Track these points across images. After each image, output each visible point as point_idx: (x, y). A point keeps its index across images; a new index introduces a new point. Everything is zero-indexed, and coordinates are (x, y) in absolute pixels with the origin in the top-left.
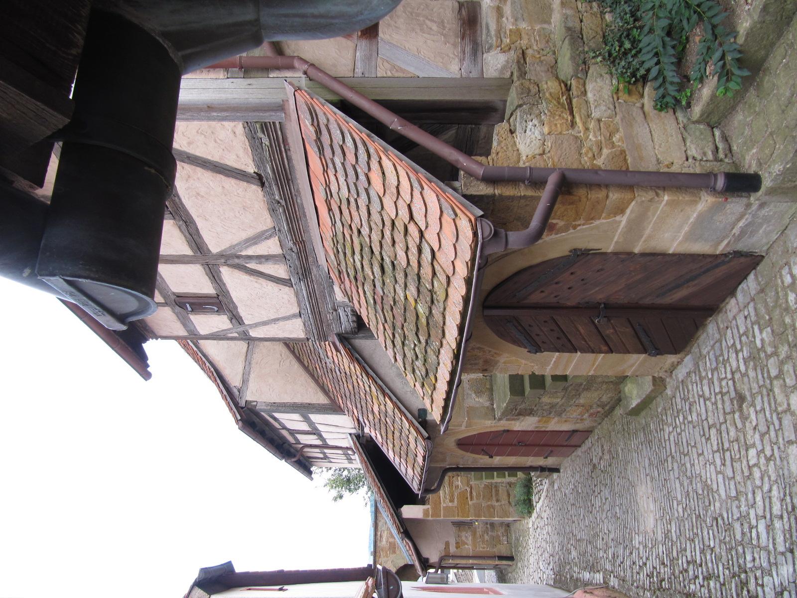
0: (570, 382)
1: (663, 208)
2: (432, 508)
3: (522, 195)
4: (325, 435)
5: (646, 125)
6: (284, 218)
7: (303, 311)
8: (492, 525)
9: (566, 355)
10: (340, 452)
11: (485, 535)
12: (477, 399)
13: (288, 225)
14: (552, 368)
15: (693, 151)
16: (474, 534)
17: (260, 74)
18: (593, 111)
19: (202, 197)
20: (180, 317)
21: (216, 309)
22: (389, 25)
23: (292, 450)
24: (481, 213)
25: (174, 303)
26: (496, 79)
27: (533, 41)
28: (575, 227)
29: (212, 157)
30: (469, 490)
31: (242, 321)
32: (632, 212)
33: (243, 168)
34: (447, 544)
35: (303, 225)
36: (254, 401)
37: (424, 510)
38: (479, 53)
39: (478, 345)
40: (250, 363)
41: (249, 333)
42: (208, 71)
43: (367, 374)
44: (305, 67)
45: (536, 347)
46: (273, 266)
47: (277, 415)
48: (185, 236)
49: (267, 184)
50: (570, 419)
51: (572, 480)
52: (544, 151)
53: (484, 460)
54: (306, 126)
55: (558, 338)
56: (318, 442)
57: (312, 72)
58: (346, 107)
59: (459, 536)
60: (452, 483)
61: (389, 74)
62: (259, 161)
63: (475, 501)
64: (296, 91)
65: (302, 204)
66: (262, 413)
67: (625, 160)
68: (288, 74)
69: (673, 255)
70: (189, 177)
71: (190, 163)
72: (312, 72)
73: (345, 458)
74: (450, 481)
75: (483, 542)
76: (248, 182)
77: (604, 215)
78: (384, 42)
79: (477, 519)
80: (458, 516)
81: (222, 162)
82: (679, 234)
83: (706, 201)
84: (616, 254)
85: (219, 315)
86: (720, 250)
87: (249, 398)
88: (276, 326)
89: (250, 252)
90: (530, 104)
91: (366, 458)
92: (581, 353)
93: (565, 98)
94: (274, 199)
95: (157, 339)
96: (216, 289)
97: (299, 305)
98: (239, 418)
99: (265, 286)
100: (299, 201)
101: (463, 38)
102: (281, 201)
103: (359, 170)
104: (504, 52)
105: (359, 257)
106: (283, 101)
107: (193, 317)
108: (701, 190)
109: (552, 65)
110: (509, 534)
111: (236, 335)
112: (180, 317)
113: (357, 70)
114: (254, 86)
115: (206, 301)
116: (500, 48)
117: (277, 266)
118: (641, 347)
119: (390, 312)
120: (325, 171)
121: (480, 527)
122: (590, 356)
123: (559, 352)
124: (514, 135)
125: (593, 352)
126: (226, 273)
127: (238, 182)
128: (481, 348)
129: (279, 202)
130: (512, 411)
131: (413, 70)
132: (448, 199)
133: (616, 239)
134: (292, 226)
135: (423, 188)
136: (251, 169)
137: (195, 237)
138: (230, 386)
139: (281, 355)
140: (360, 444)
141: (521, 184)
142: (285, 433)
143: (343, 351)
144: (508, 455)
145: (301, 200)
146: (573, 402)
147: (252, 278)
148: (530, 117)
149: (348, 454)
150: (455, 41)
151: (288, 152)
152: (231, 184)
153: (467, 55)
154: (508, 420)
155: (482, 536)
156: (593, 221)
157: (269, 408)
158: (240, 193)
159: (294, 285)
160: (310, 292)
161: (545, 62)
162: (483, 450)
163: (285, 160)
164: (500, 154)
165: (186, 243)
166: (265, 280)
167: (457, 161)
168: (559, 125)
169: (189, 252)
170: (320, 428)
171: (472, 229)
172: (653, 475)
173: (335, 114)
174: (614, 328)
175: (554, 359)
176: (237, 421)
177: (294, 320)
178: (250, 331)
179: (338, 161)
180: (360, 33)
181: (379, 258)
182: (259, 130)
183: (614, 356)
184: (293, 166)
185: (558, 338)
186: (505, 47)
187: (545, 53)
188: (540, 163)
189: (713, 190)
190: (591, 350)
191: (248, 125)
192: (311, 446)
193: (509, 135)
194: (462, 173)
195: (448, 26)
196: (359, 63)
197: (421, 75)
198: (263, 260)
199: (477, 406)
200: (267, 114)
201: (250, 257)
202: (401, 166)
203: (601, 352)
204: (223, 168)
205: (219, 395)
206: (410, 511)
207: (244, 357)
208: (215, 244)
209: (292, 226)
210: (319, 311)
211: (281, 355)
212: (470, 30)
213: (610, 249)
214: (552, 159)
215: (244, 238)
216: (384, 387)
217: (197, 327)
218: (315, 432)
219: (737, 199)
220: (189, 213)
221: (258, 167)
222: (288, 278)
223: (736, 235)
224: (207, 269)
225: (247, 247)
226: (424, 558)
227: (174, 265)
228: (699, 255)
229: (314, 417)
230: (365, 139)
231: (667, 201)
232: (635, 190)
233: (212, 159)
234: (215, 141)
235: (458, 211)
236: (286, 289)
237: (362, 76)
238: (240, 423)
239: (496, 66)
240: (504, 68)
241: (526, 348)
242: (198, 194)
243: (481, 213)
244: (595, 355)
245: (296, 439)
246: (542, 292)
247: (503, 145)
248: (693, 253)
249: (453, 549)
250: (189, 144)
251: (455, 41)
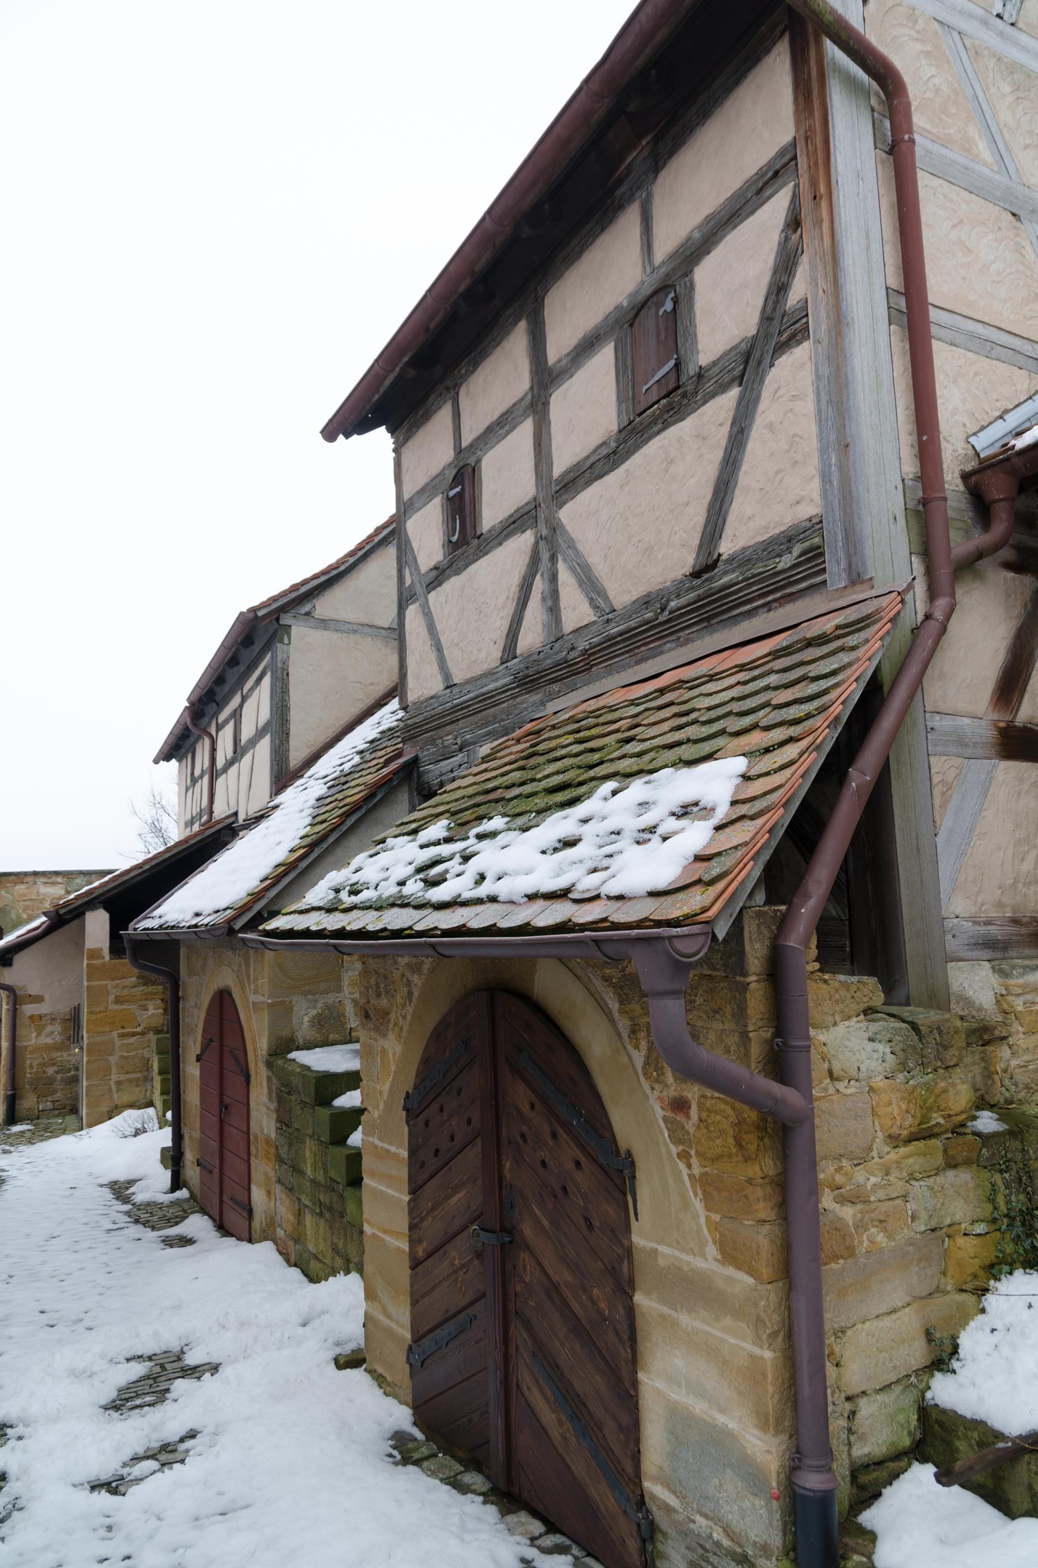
0: (349, 1192)
1: (744, 1349)
2: (104, 964)
3: (751, 1035)
4: (233, 770)
5: (907, 1299)
6: (632, 624)
7: (456, 690)
8: (75, 1080)
9: (404, 1173)
10: (205, 803)
11: (56, 1068)
12: (306, 1019)
13: (621, 635)
14: (376, 1147)
15: (866, 1408)
16: (58, 1047)
17: (915, 538)
18: (922, 1183)
19: (666, 470)
20: (437, 481)
21: (455, 539)
22: (1021, 780)
23: (205, 720)
24: (721, 936)
25: (461, 464)
26: (947, 986)
27: (1025, 1058)
28: (684, 1156)
29: (746, 473)
30: (139, 1029)
31: (434, 588)
32: (729, 1280)
33: (728, 531)
34: (38, 999)
35: (622, 663)
36: (289, 640)
37: (101, 949)
38: (987, 954)
39: (416, 993)
40: (355, 631)
41: (412, 603)
42: (912, 445)
43: (347, 815)
44: (939, 615)
45: (416, 1107)
46: (540, 622)
47: (267, 680)
48: (588, 457)
49: (698, 581)
50: (273, 1201)
51: (155, 1218)
52: (838, 1079)
53: (192, 1046)
54: (834, 619)
55: (437, 1151)
56: (220, 762)
57: (933, 626)
58: (873, 698)
59: (53, 1019)
60: (151, 999)
61: (936, 779)
62: (743, 559)
63: (118, 1043)
64: (899, 593)
65: (662, 653)
66: (269, 655)
67: (837, 1257)
68: (920, 588)
69: (635, 1383)
70: (704, 438)
71: (730, 436)
72: (933, 626)
73: (194, 814)
74: (155, 994)
75: (42, 1065)
76: (700, 546)
77: (716, 1217)
78: (992, 770)
79: (85, 1047)
80: (89, 1013)
81: (737, 492)
82: (684, 1391)
83: (765, 1449)
84: (629, 1251)
85: (443, 546)
86: (654, 1489)
87: (295, 631)
88: (427, 648)
89: (565, 576)
90: (922, 1049)
91: (193, 842)
92: (409, 1202)
93: (941, 1121)
94: (668, 600)
95: (394, 451)
96: (490, 531)
97: (468, 682)
98: (260, 614)
99: (501, 615)
100: (668, 646)
101: (1015, 921)
102: (666, 613)
103: (762, 713)
104: (998, 1001)
105: (574, 751)
106: (871, 579)
107: (437, 501)
108: (791, 1437)
109: (987, 1097)
110: (57, 1112)
111: (408, 581)
112: (437, 481)
113: (937, 718)
114: (892, 526)
115: (468, 519)
116: (1004, 992)
117: (539, 628)
118: (427, 1328)
119: (474, 816)
120: (742, 668)
121: (70, 1058)
122: (402, 1222)
123: (410, 1157)
124: (862, 1017)
125: (412, 1227)
126: (523, 542)
127: (700, 528)
128: (410, 1001)
129: (663, 610)
130: (286, 1086)
131: (946, 822)
132: (741, 865)
133: (662, 1249)
134: (618, 643)
135: (752, 818)
136: (727, 547)
137: (587, 475)
138: (314, 598)
139: (371, 684)
140: (219, 831)
141: (772, 1030)
142: (236, 700)
143: (385, 771)
144: (201, 1088)
145: (670, 650)
146: (308, 1203)
147: (514, 588)
148: (897, 1049)
149: (201, 818)
150: (1006, 906)
151: (765, 609)
152: (697, 516)
153: (983, 929)
154: (269, 1079)
155: (52, 1062)
156: (700, 1195)
157: (279, 665)
158: (677, 536)
159: (505, 665)
160: (493, 696)
161: (990, 1082)
162: (211, 1040)
163: (749, 607)
164: (825, 987)
165: (575, 460)
166: (512, 612)
167: (807, 896)
168: (889, 1109)
169: (558, 470)
170: (247, 759)
171: (687, 917)
172: (163, 1378)
173: (869, 659)
174: (463, 1266)
175: (393, 1149)
176: (253, 610)
177: (439, 677)
178: (417, 604)
179: (773, 679)
180: (1002, 725)
181: (581, 779)
182: (807, 544)
183: (403, 1272)
184: (736, 624)
185: (437, 1151)
186: (1009, 1004)
187: (1007, 1082)
188: (818, 1070)
189: (795, 1464)
190: (415, 1222)
191: (816, 525)
192: (213, 750)
193: (862, 1007)
194: (783, 908)
195: (1031, 892)
196: (950, 723)
197: (940, 840)
198: (550, 603)
199: (294, 1020)
200: (841, 554)
201: (553, 578)
202: (793, 775)
203: (413, 1242)
204: (725, 496)
205: (298, 580)
206: (97, 925)
207: (366, 621)
208: (572, 514)
209: (618, 643)
210: (458, 720)
211: (371, 684)
212: (1029, 935)
213: (638, 1240)
214: (823, 1097)
215: (590, 560)
216: (325, 845)
217: (419, 514)
218: (239, 751)
219: (777, 1523)
220: (633, 454)
221: (731, 559)
222: (518, 652)
223: (692, 1525)
224: (527, 509)
225: (573, 570)
226: (11, 959)
227: (532, 450)
228: (637, 1441)
229: (265, 745)
230: (832, 709)
231: (762, 1358)
232: (780, 1284)
233: (741, 473)
234: (777, 473)
235: (720, 886)
236: (497, 653)
237: (929, 727)
238: (252, 615)
239: (970, 986)
240: (969, 1002)
241: (415, 1088)
242: (672, 461)
243: (721, 936)
244: (407, 1231)
245: (226, 722)
246: (533, 1106)
247: (843, 992)
248: (642, 1428)
249: (28, 1009)
250: (771, 427)
251: (1006, 906)
